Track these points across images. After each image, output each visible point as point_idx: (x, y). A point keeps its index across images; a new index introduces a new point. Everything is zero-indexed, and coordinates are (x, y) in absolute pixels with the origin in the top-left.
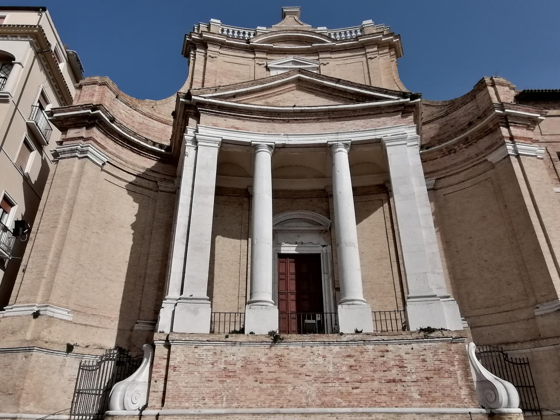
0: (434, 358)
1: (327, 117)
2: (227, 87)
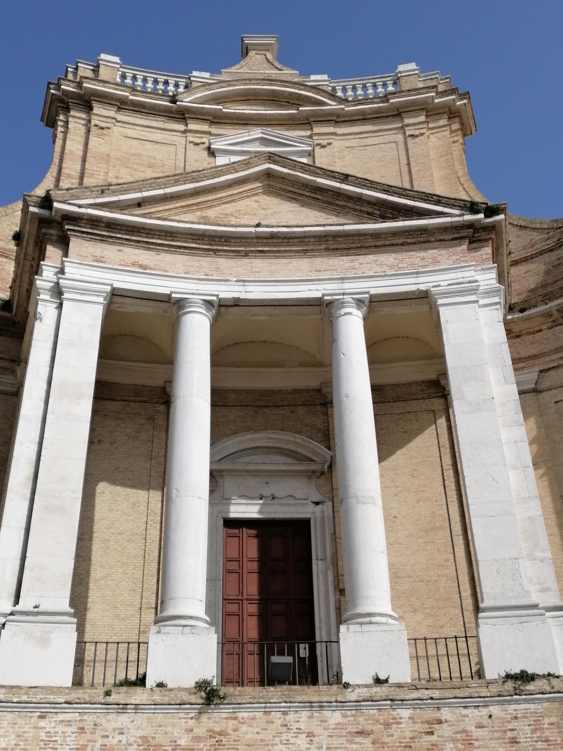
0: (535, 736)
1: (323, 247)
2: (125, 187)
